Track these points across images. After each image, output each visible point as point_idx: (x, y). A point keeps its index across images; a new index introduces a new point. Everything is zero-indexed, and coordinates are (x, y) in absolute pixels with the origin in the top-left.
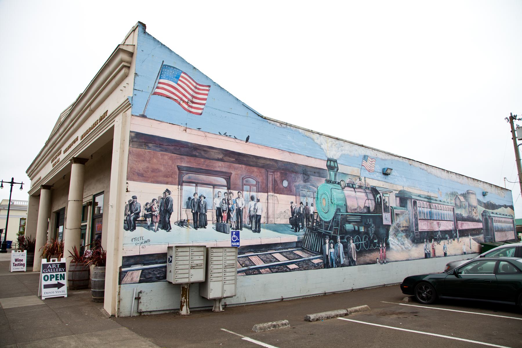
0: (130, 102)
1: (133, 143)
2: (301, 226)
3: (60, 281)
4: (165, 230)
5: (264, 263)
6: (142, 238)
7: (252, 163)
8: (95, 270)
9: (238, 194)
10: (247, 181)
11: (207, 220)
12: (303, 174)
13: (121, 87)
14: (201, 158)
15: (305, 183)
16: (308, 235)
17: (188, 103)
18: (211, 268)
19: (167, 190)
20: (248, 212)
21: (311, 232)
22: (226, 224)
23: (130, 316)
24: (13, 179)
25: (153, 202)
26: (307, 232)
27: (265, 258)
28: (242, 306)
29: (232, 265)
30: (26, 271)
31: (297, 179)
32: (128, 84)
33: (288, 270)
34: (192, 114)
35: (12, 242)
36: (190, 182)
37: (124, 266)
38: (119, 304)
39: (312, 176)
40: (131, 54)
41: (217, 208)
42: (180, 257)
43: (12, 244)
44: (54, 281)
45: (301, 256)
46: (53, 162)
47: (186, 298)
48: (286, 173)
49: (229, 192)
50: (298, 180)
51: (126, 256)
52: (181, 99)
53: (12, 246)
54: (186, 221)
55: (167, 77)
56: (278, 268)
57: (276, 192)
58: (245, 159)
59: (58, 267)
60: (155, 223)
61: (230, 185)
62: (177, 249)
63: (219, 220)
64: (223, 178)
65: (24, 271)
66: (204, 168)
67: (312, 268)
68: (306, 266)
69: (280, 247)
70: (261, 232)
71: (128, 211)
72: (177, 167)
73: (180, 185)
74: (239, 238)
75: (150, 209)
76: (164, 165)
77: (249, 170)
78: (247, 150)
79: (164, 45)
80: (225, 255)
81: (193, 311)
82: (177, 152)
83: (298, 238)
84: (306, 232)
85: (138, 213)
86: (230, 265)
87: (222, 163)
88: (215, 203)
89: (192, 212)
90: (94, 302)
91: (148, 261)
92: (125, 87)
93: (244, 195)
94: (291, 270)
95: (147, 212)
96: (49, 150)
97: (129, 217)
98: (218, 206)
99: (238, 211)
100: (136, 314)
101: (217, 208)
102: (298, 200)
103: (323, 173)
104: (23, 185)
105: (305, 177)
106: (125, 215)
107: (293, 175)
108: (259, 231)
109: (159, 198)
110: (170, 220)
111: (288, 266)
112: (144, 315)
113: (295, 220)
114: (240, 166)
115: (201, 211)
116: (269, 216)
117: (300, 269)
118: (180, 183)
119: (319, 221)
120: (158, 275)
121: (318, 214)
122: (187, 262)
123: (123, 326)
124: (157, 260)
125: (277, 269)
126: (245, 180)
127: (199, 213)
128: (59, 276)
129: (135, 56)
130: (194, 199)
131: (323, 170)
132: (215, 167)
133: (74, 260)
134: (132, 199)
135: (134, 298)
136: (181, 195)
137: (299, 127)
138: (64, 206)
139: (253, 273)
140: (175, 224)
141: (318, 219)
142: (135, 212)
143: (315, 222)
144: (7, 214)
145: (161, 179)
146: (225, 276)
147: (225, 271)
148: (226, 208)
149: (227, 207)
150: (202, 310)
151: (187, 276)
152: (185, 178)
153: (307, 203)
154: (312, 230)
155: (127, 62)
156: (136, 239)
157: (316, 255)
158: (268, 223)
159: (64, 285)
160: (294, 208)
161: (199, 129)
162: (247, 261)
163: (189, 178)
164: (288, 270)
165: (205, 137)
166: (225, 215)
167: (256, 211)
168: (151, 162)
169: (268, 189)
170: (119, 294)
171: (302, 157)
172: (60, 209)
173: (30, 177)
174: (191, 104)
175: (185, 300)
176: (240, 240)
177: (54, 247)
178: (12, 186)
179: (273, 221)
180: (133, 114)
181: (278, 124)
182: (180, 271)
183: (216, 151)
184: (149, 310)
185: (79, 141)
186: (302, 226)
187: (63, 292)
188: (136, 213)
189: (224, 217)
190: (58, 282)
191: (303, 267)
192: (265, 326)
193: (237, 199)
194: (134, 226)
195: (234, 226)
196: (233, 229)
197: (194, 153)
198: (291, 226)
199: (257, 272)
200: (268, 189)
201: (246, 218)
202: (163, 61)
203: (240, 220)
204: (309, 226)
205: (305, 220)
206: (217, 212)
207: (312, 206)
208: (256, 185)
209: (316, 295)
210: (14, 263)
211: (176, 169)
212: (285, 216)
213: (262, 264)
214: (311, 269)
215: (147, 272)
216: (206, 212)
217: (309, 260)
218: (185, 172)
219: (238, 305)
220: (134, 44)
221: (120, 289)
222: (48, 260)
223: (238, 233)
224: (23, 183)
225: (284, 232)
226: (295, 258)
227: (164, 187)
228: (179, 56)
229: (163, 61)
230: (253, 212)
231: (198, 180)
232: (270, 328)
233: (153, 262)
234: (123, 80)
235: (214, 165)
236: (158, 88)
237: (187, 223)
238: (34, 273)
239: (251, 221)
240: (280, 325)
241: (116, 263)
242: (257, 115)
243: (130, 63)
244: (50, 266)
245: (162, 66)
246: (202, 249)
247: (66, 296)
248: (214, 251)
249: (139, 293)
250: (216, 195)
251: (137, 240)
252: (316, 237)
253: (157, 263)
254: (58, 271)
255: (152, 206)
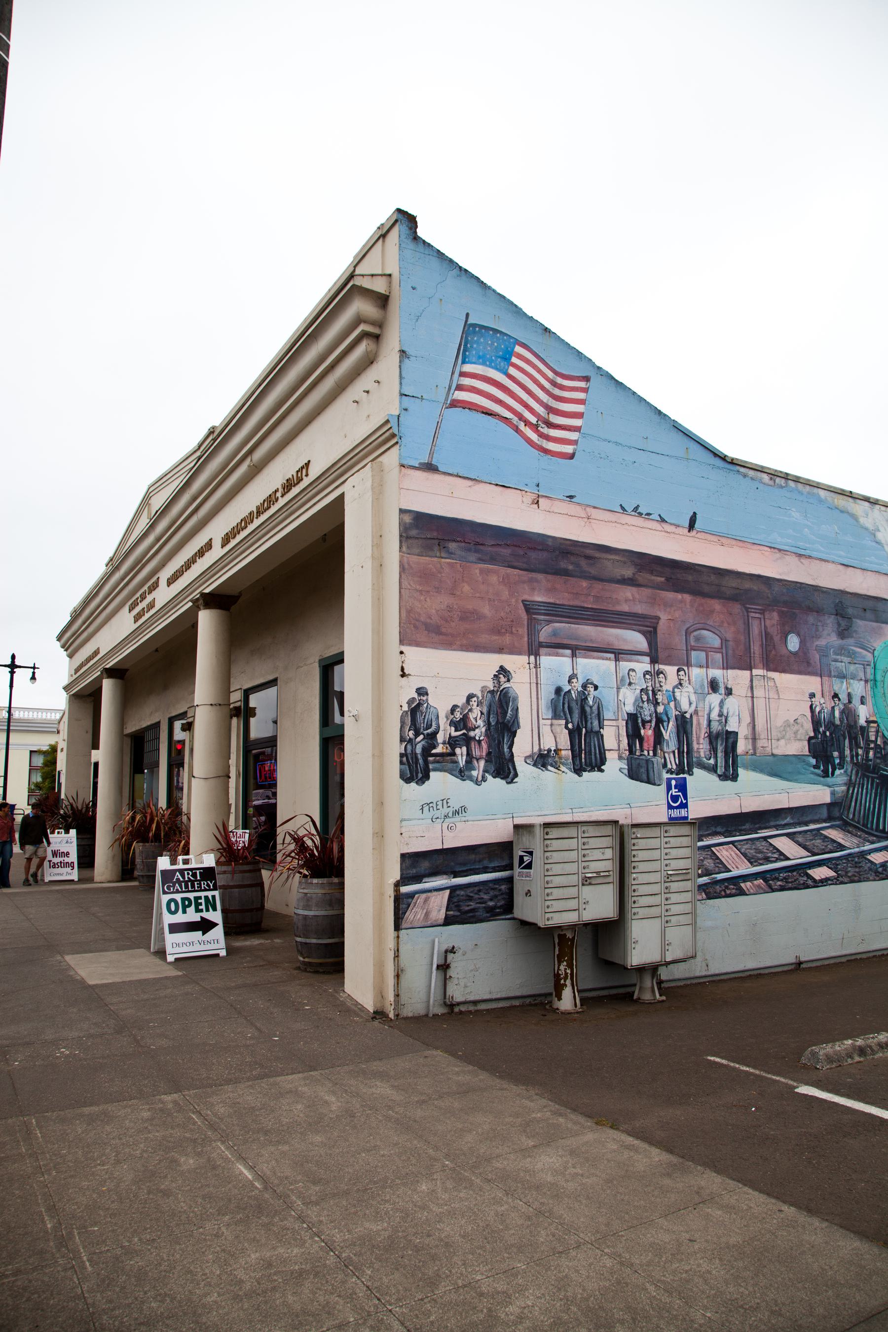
0: (395, 430)
1: (410, 541)
2: (837, 761)
3: (205, 915)
4: (502, 779)
5: (751, 863)
6: (447, 803)
7: (706, 589)
8: (304, 889)
9: (678, 675)
10: (698, 639)
11: (605, 750)
12: (837, 615)
13: (355, 391)
14: (580, 577)
15: (842, 639)
16: (857, 786)
17: (537, 426)
18: (633, 882)
19: (503, 670)
20: (705, 723)
21: (863, 776)
22: (653, 759)
23: (427, 1015)
24: (13, 657)
25: (469, 704)
26: (853, 777)
27: (752, 851)
28: (699, 983)
29: (684, 871)
30: (79, 880)
31: (820, 629)
32: (378, 382)
33: (811, 884)
34: (550, 457)
35: (16, 807)
36: (556, 646)
37: (406, 880)
38: (398, 984)
39: (858, 621)
40: (383, 301)
41: (628, 714)
42: (554, 854)
43: (16, 812)
44: (192, 916)
45: (840, 844)
46: (133, 608)
47: (570, 965)
48: (794, 613)
49: (656, 669)
50: (825, 632)
51: (409, 851)
52: (521, 417)
53: (15, 816)
54: (553, 752)
55: (479, 357)
56: (785, 878)
57: (771, 665)
58: (690, 578)
59: (199, 878)
60: (477, 760)
61: (657, 650)
62: (546, 830)
63: (636, 747)
64: (639, 631)
65: (73, 880)
66: (590, 606)
67: (869, 875)
68: (855, 872)
69: (788, 820)
70: (739, 779)
71: (409, 730)
72: (521, 604)
73: (532, 655)
74: (686, 797)
75: (462, 723)
76: (490, 600)
77: (701, 608)
78: (692, 553)
79: (466, 271)
80: (666, 846)
81: (588, 1001)
82: (520, 564)
83: (833, 794)
84: (851, 777)
85: (435, 734)
86: (680, 872)
87: (634, 589)
88: (623, 701)
89: (566, 727)
90: (305, 970)
91: (465, 864)
92: (368, 392)
93: (693, 679)
94: (818, 883)
95: (456, 730)
96: (122, 579)
97: (412, 745)
98: (630, 708)
99: (679, 722)
100: (440, 1011)
101: (628, 714)
102: (826, 688)
103: (884, 612)
104: (36, 670)
105: (841, 622)
106: (402, 740)
107: (811, 619)
108: (734, 778)
109: (482, 691)
110: (514, 750)
111: (810, 872)
112: (461, 1012)
113: (822, 742)
114: (679, 596)
115: (589, 724)
116: (757, 733)
117: (840, 879)
118: (532, 649)
119: (882, 746)
120: (491, 904)
121: (878, 725)
122: (572, 868)
123: (428, 1045)
124: (486, 863)
125: (782, 880)
126: (692, 635)
127: (584, 729)
128: (203, 901)
129: (395, 305)
130: (569, 691)
131: (884, 601)
132: (618, 602)
133: (223, 859)
134: (416, 696)
135: (435, 966)
136: (537, 681)
137: (818, 483)
138: (157, 720)
139: (723, 893)
140: (526, 762)
141: (879, 739)
142: (425, 732)
143: (872, 748)
144: (5, 741)
145: (484, 638)
146: (669, 902)
147: (667, 888)
148: (651, 715)
149: (653, 711)
150: (606, 996)
151: (573, 904)
152: (545, 633)
153: (849, 695)
154: (866, 771)
155: (373, 323)
156: (431, 805)
157: (879, 842)
158: (754, 754)
159: (214, 925)
160: (818, 709)
161: (571, 497)
162: (707, 858)
163: (555, 634)
164: (811, 884)
165: (586, 520)
166: (648, 733)
167: (724, 721)
168: (458, 593)
169: (750, 660)
170: (398, 956)
171: (831, 566)
172: (144, 726)
173: (66, 650)
174: (545, 430)
175: (569, 971)
176: (689, 804)
177: (146, 822)
178: (12, 673)
179: (767, 749)
180: (405, 462)
181: (766, 478)
182: (557, 893)
183: (617, 558)
184: (472, 998)
185: (217, 552)
186: (840, 759)
187: (216, 941)
188: (428, 734)
189: (646, 739)
190: (202, 917)
191: (846, 875)
192: (839, 1051)
193: (676, 690)
194: (424, 770)
195: (672, 764)
196: (670, 771)
197: (563, 564)
198: (813, 761)
199: (734, 891)
200: (752, 658)
201: (701, 741)
202: (467, 315)
203: (685, 746)
204: (857, 759)
205: (847, 742)
206: (630, 726)
207: (862, 703)
208: (722, 648)
209: (880, 953)
210: (50, 861)
211: (520, 611)
212: (796, 733)
213: (745, 868)
214: (868, 880)
215: (462, 896)
216: (601, 726)
217: (863, 854)
218: (542, 617)
219: (689, 982)
220: (388, 272)
221: (398, 943)
222: (174, 862)
223: (682, 782)
224: (36, 666)
225: (795, 778)
226: (826, 850)
227: (491, 662)
228: (504, 297)
229: (467, 315)
230: (718, 723)
231: (577, 639)
232: (852, 1058)
233: (477, 867)
234: (359, 375)
235: (614, 596)
236: (460, 388)
237: (557, 759)
238: (100, 885)
239: (713, 749)
240: (875, 1048)
241: (380, 871)
242: (711, 455)
243: (380, 324)
244: (180, 877)
245: (466, 328)
246: (608, 830)
247: (223, 953)
248: (639, 836)
249: (446, 952)
250: (622, 680)
251: (435, 809)
252: (876, 790)
253: (485, 870)
254: (198, 887)
255: (468, 713)
